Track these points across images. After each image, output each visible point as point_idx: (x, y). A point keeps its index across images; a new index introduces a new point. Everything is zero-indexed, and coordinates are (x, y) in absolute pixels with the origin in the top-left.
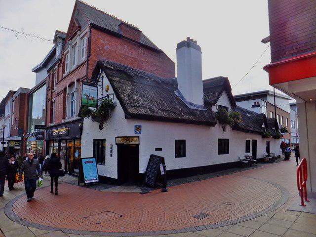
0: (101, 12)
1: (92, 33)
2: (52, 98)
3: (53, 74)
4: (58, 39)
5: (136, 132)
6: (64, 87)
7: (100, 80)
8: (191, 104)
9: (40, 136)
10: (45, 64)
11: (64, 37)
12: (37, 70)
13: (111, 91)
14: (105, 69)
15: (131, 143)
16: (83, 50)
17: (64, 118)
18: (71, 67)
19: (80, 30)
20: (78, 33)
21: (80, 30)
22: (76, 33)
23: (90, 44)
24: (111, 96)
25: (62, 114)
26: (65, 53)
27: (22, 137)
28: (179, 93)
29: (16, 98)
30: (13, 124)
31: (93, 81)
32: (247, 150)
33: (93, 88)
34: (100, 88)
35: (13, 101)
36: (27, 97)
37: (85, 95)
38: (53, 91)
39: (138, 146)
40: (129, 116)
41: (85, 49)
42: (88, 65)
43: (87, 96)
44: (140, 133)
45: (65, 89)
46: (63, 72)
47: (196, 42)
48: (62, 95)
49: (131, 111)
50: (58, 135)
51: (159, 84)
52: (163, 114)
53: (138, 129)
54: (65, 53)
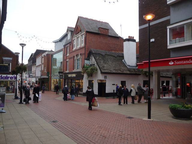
0: (90, 19)
1: (87, 35)
2: (66, 59)
3: (67, 48)
4: (69, 31)
5: (105, 78)
6: (73, 56)
7: (91, 57)
8: (129, 66)
9: (61, 77)
10: (61, 40)
11: (73, 30)
12: (56, 42)
13: (95, 63)
14: (93, 54)
15: (103, 82)
16: (82, 41)
17: (74, 69)
18: (77, 47)
19: (81, 31)
20: (80, 33)
21: (81, 31)
22: (79, 32)
23: (86, 40)
24: (95, 65)
25: (73, 68)
26: (73, 39)
27: (49, 76)
28: (125, 61)
29: (44, 56)
30: (43, 69)
31: (88, 59)
32: (20, 77)
33: (88, 61)
34: (91, 61)
35: (42, 57)
36: (51, 56)
37: (86, 64)
38: (67, 56)
39: (106, 83)
40: (102, 73)
41: (83, 40)
42: (85, 49)
43: (86, 64)
44: (106, 78)
45: (74, 56)
46: (73, 48)
47: (133, 37)
48: (72, 60)
49: (103, 71)
50: (71, 77)
51: (116, 57)
52: (114, 71)
53: (105, 77)
54: (73, 39)
